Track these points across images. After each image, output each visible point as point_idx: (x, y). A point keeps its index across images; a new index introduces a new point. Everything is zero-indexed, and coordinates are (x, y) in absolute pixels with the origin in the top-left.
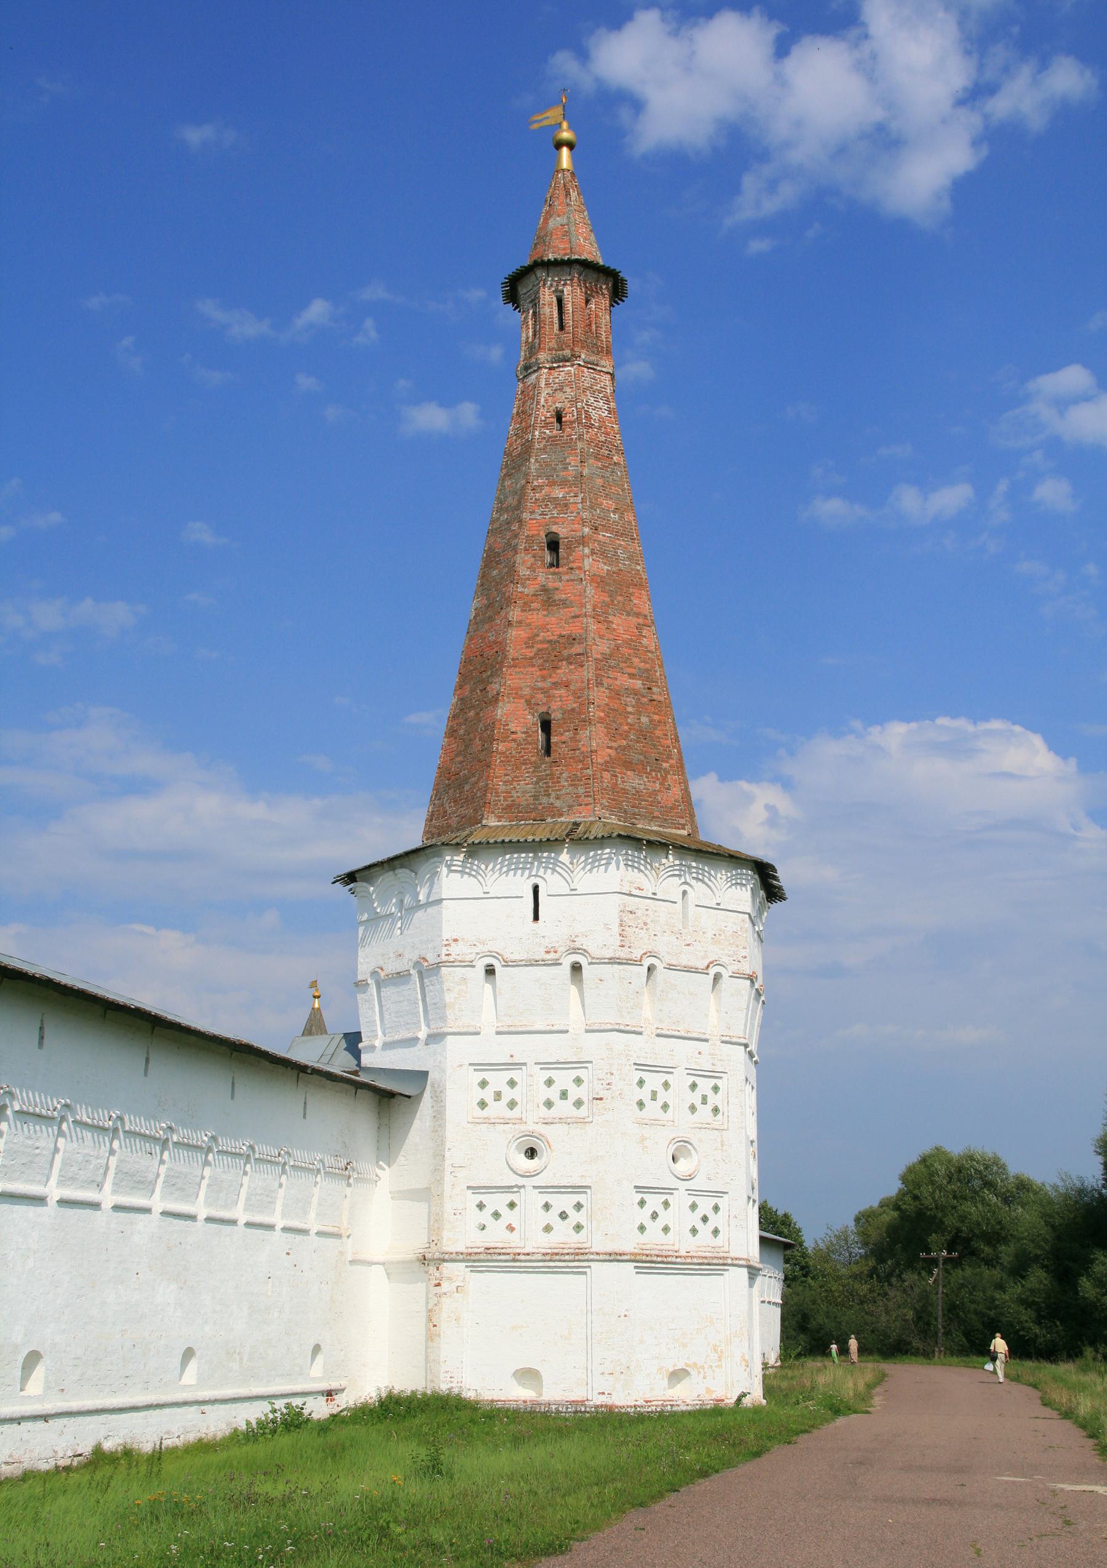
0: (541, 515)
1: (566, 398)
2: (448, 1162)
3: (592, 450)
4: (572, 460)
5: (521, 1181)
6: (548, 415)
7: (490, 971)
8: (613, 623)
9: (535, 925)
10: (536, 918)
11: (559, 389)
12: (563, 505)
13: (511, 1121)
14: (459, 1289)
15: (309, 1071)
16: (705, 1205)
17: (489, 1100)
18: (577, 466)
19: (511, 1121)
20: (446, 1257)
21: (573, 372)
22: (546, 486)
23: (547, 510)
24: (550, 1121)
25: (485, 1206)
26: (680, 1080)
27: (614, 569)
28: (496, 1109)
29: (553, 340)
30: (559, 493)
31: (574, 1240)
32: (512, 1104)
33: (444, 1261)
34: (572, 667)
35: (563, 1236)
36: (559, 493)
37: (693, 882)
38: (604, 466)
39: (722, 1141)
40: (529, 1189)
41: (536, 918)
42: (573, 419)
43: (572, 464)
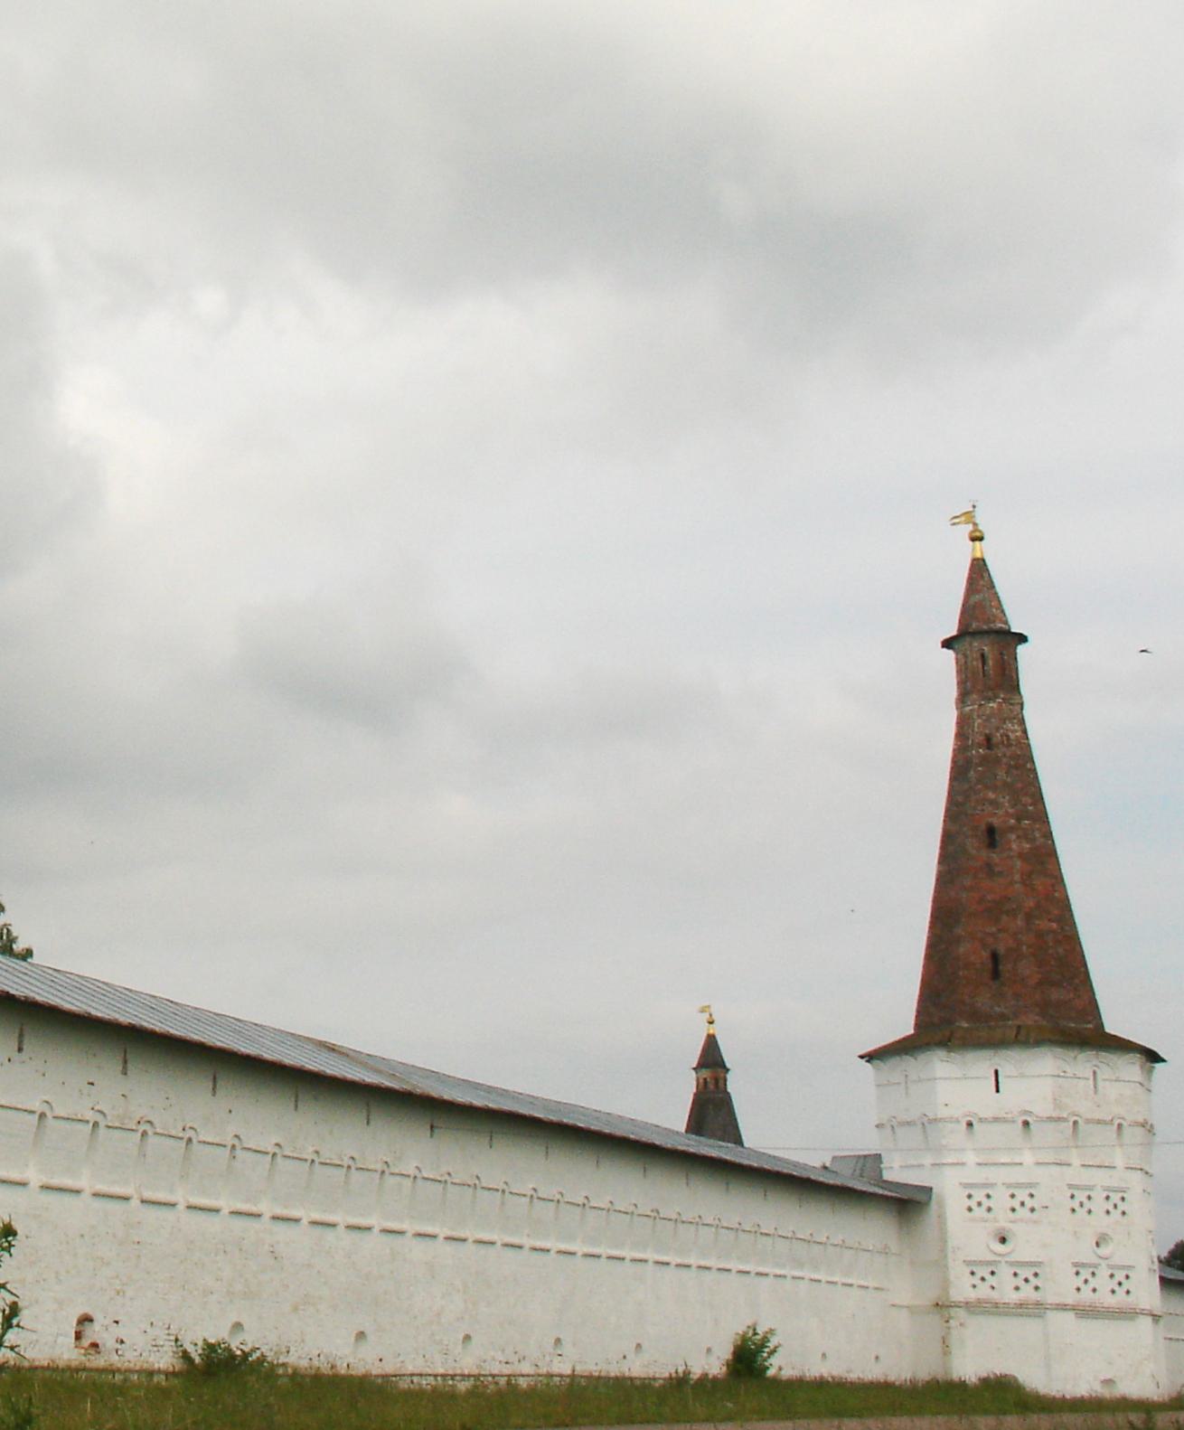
5: (999, 1259)
7: (970, 1124)
9: (998, 1094)
10: (998, 1091)
12: (994, 803)
16: (1120, 1276)
17: (974, 1207)
20: (953, 1304)
26: (1099, 1196)
28: (979, 1212)
31: (1034, 1296)
32: (989, 1209)
33: (951, 1306)
35: (1027, 1293)
36: (991, 795)
37: (1100, 1064)
40: (1003, 1263)
41: (998, 1091)
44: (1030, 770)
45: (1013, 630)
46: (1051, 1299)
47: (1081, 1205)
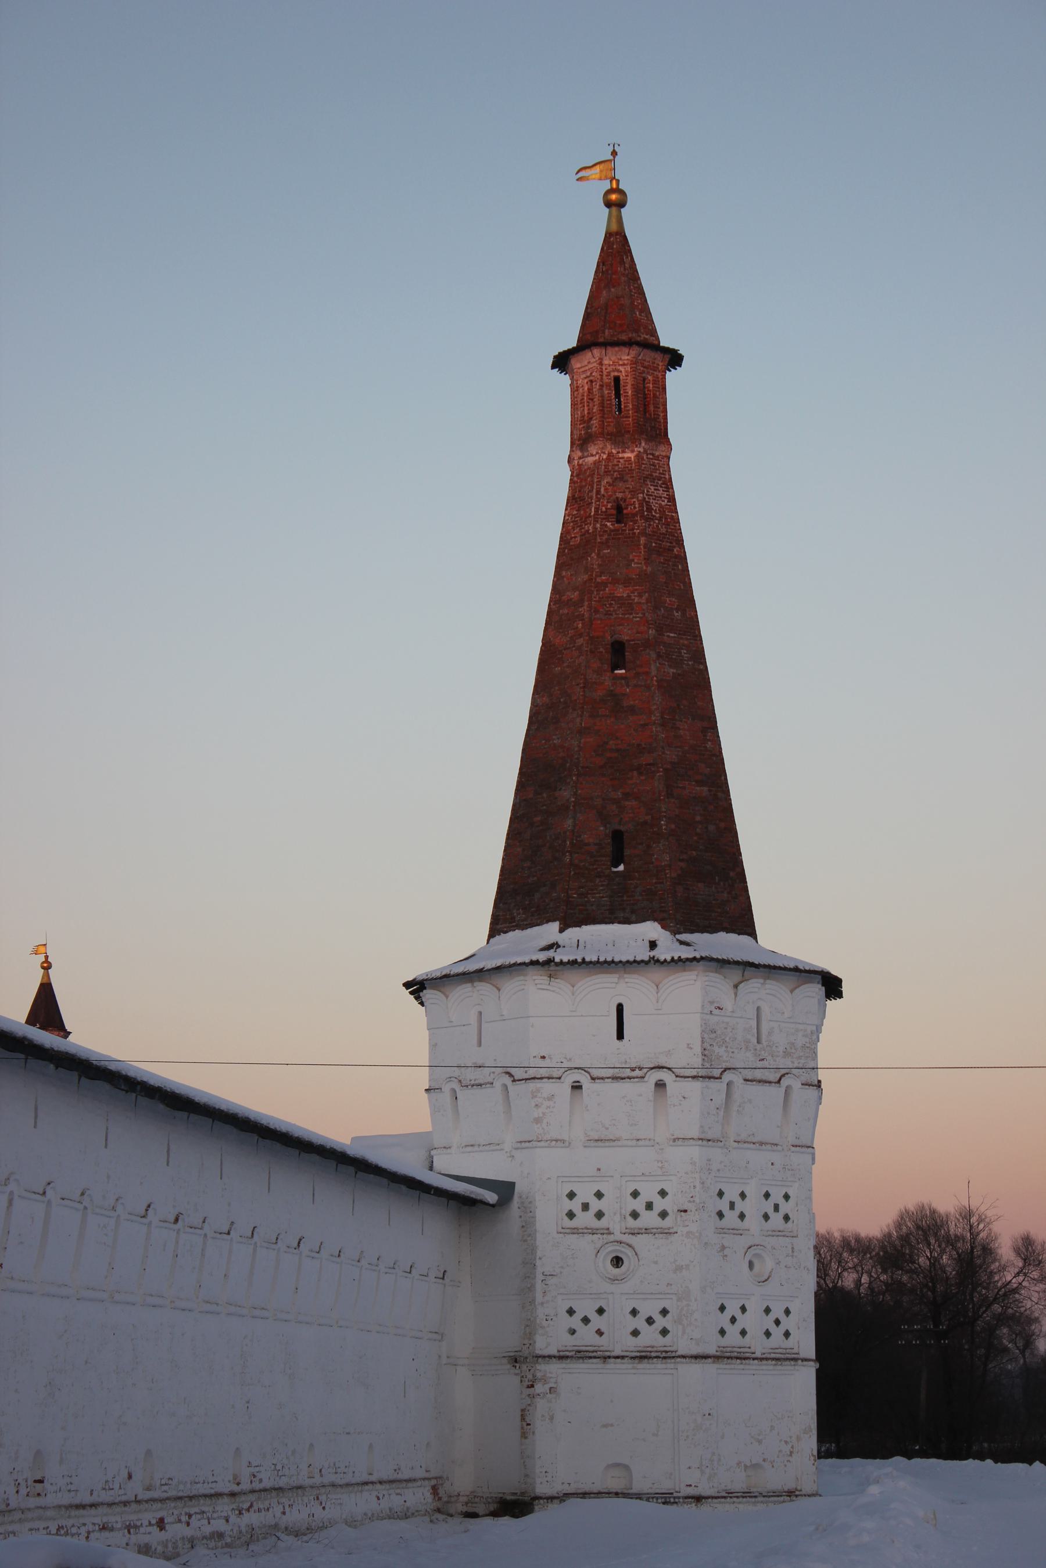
0: (606, 615)
1: (627, 488)
2: (539, 1270)
3: (654, 545)
4: (635, 556)
6: (609, 506)
8: (679, 729)
10: (620, 1036)
11: (620, 478)
13: (598, 1232)
14: (552, 1390)
15: (139, 1087)
18: (641, 564)
19: (598, 1232)
21: (633, 459)
22: (610, 583)
23: (612, 609)
24: (636, 1231)
25: (575, 1312)
27: (680, 672)
29: (612, 424)
30: (621, 591)
31: (661, 1342)
32: (600, 1215)
34: (643, 778)
35: (650, 1337)
38: (666, 560)
39: (793, 1248)
41: (620, 1036)
42: (634, 511)
43: (636, 561)
44: (676, 557)
45: (662, 344)
46: (684, 1347)
47: (732, 1205)
